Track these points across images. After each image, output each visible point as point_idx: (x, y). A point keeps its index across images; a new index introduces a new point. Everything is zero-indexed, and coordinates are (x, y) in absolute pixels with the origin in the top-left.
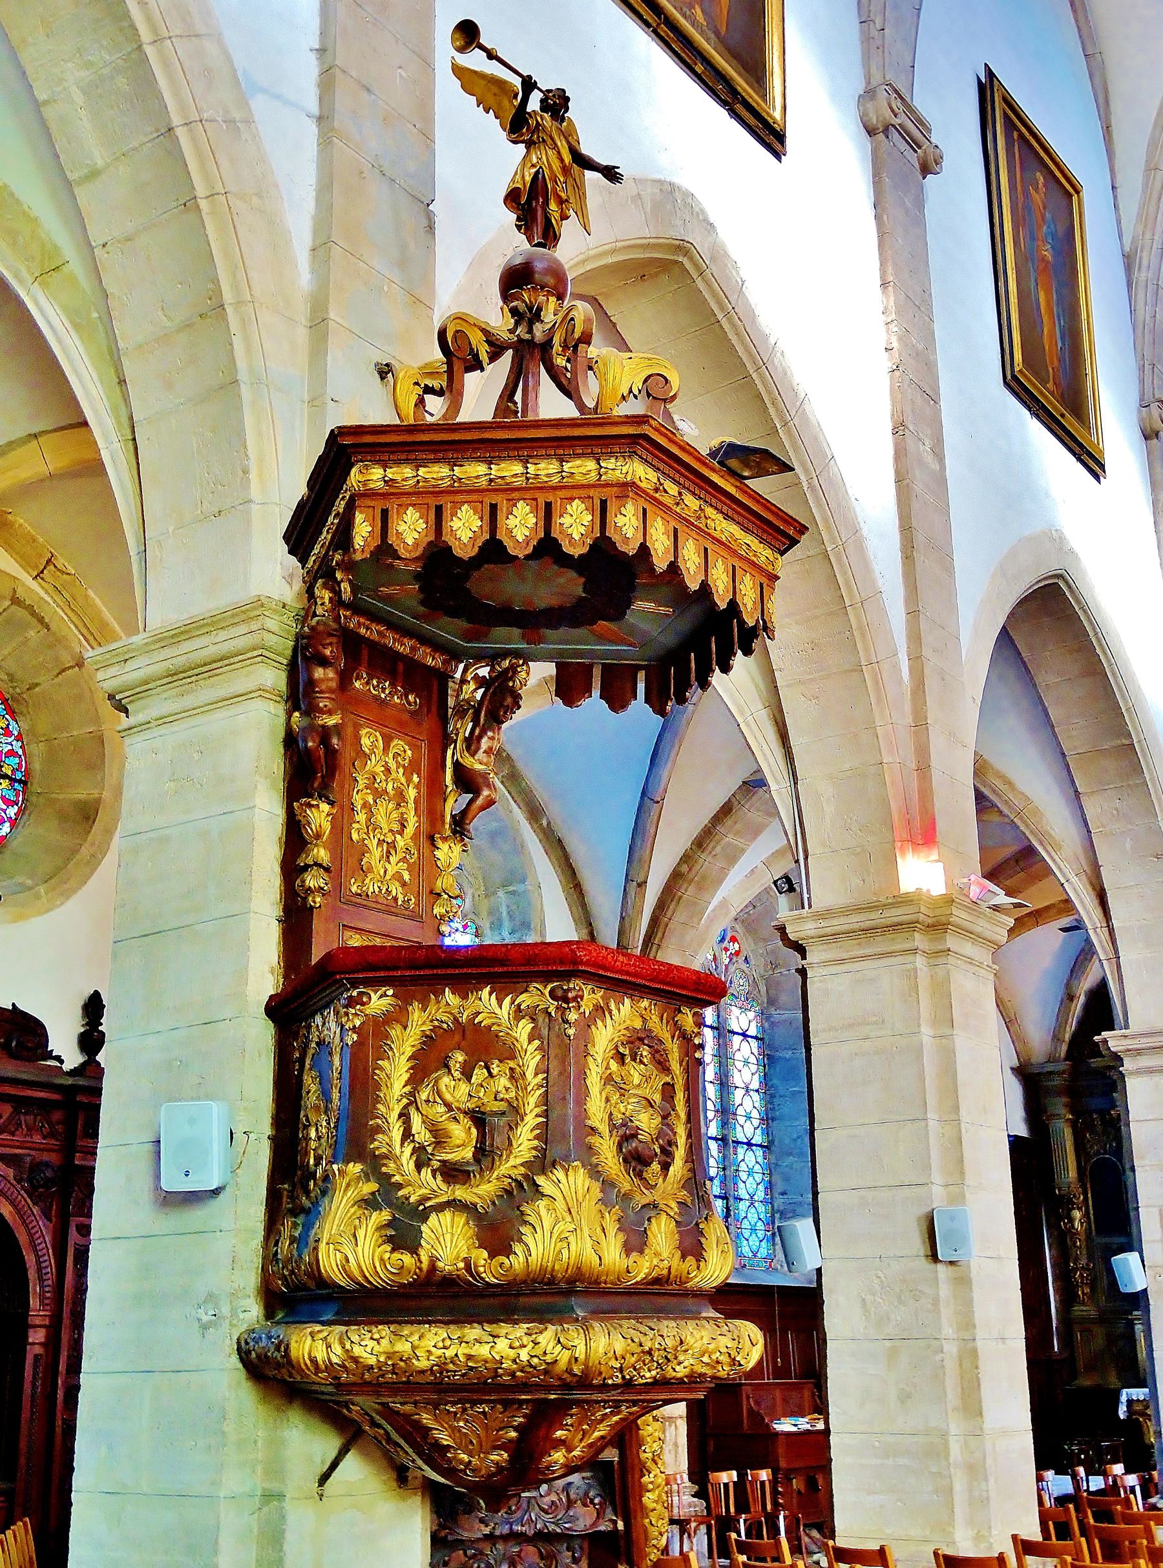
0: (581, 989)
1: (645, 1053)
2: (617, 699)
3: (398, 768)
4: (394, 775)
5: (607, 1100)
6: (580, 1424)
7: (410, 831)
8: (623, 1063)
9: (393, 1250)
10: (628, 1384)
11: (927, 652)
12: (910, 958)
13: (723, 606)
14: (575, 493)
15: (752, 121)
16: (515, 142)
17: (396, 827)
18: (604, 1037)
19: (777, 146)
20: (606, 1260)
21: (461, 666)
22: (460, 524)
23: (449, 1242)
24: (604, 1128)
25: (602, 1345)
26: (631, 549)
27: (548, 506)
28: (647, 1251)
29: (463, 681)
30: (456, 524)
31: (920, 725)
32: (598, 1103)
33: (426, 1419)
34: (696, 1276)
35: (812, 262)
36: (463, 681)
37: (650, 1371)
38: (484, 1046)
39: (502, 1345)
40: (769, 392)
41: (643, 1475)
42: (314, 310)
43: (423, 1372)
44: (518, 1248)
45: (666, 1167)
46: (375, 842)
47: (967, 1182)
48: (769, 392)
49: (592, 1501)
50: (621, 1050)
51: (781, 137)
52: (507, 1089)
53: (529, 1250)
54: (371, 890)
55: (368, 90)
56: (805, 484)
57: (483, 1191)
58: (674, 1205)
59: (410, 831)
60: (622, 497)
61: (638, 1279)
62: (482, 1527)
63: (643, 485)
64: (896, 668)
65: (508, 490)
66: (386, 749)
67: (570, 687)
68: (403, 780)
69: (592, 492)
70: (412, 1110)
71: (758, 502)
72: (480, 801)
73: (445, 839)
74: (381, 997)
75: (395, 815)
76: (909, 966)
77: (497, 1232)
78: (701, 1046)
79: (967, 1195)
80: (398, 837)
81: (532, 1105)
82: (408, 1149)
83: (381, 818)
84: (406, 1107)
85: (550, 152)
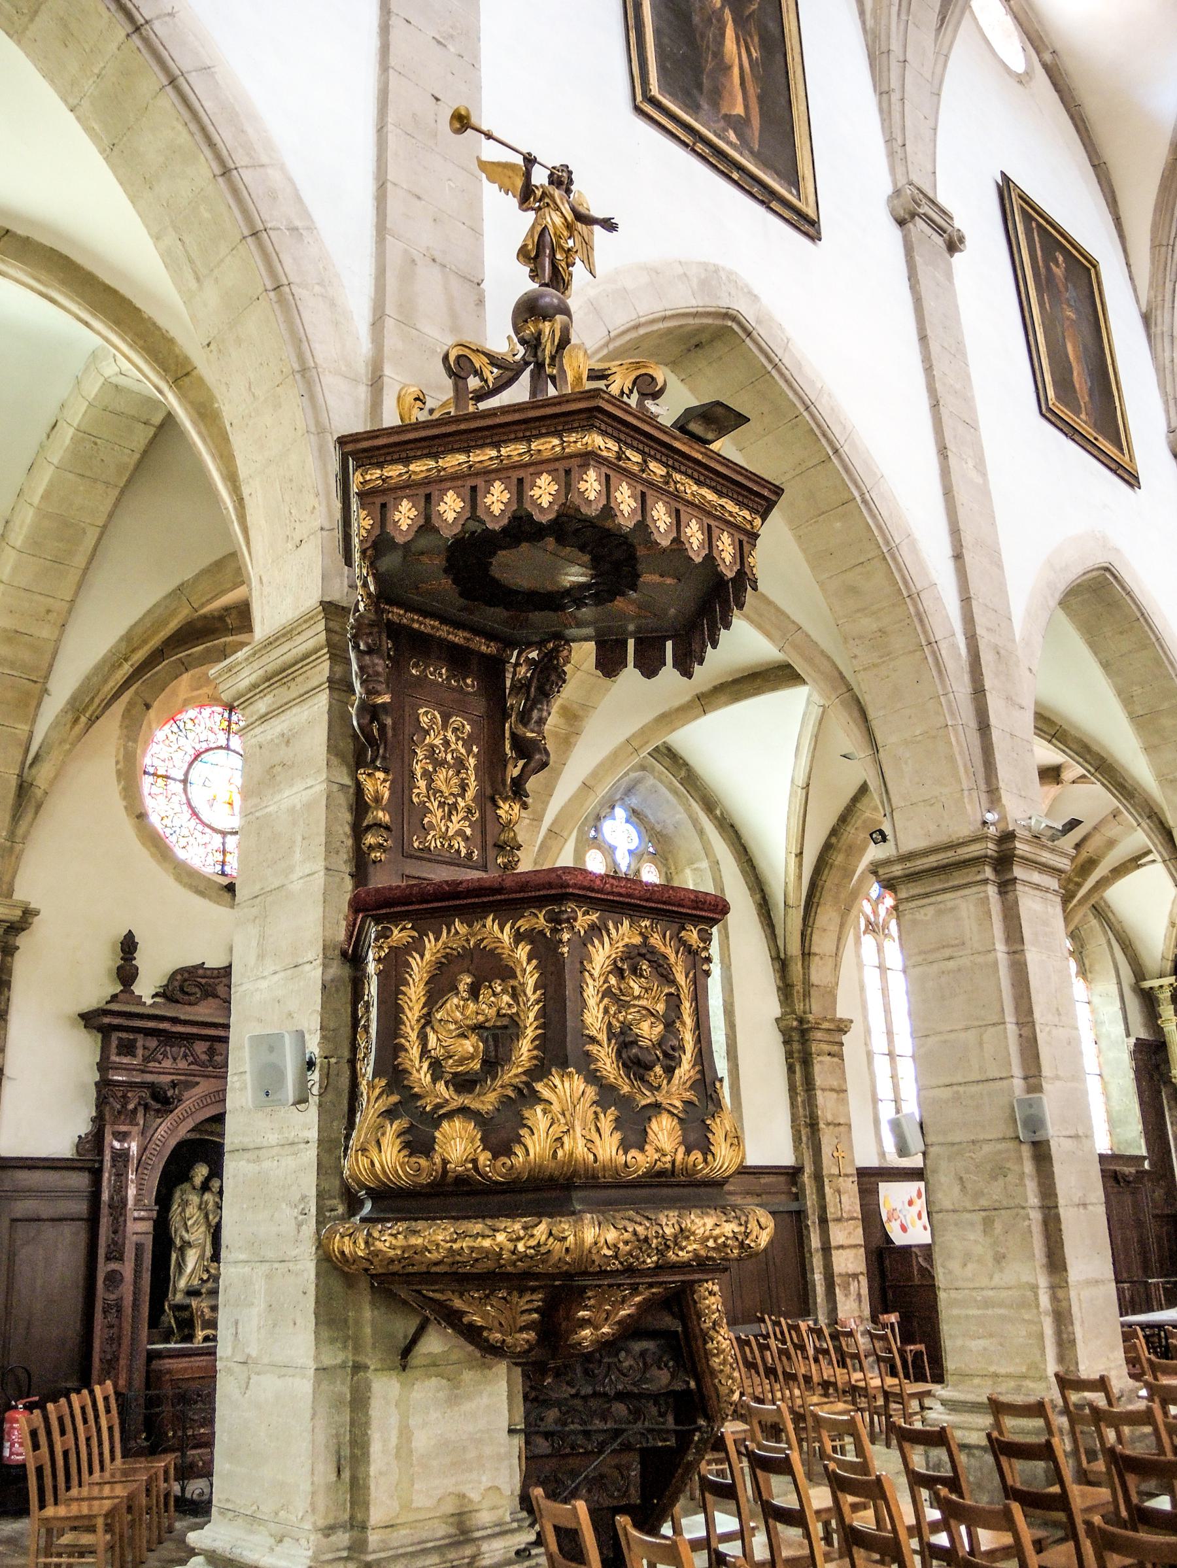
0: (573, 911)
1: (644, 967)
2: (649, 668)
3: (457, 740)
4: (453, 746)
5: (606, 1011)
6: (601, 1305)
7: (470, 794)
8: (623, 978)
9: (410, 1156)
10: (630, 1270)
11: (980, 631)
12: (982, 888)
13: (665, 542)
14: (542, 467)
15: (787, 214)
16: (525, 210)
17: (456, 790)
18: (601, 956)
19: (811, 231)
20: (600, 1158)
21: (515, 653)
22: (446, 507)
23: (458, 1144)
24: (602, 1037)
25: (594, 1234)
26: (592, 511)
27: (520, 481)
28: (647, 1147)
29: (517, 664)
30: (442, 508)
31: (979, 691)
32: (595, 1012)
33: (458, 1303)
34: (703, 1169)
35: (866, 335)
36: (517, 664)
37: (649, 1256)
38: (489, 968)
39: (501, 1237)
40: (819, 426)
41: (705, 1343)
42: (374, 372)
43: (436, 1264)
44: (519, 1150)
45: (670, 1071)
46: (436, 804)
47: (1044, 1074)
48: (819, 426)
49: (666, 1365)
50: (620, 964)
51: (814, 223)
52: (510, 1006)
53: (527, 1150)
54: (433, 844)
55: (419, 198)
56: (859, 499)
57: (487, 1101)
58: (678, 1104)
59: (470, 794)
60: (584, 466)
61: (640, 1173)
62: (569, 1389)
63: (605, 454)
64: (954, 646)
65: (485, 473)
66: (445, 726)
67: (609, 664)
68: (463, 751)
69: (557, 465)
70: (428, 1029)
71: (727, 466)
72: (532, 765)
73: (505, 800)
74: (402, 930)
75: (455, 781)
76: (982, 895)
77: (500, 1133)
78: (708, 960)
79: (1044, 1084)
80: (459, 799)
81: (531, 1019)
82: (425, 1065)
83: (440, 783)
84: (423, 1027)
85: (553, 213)
